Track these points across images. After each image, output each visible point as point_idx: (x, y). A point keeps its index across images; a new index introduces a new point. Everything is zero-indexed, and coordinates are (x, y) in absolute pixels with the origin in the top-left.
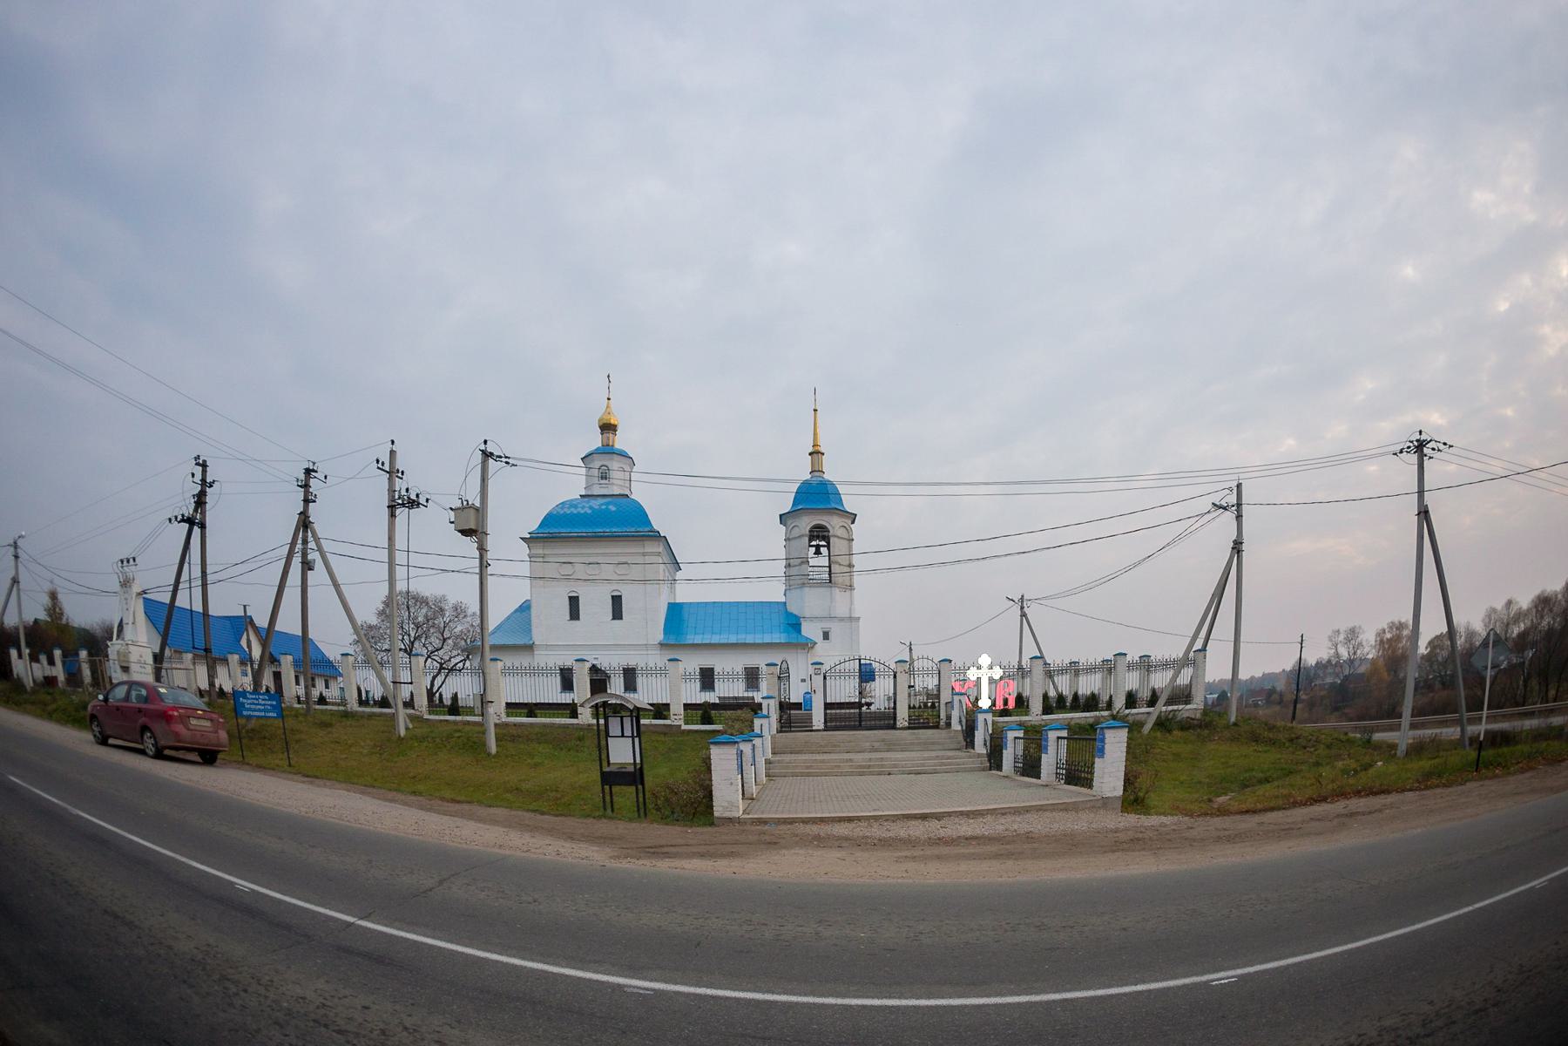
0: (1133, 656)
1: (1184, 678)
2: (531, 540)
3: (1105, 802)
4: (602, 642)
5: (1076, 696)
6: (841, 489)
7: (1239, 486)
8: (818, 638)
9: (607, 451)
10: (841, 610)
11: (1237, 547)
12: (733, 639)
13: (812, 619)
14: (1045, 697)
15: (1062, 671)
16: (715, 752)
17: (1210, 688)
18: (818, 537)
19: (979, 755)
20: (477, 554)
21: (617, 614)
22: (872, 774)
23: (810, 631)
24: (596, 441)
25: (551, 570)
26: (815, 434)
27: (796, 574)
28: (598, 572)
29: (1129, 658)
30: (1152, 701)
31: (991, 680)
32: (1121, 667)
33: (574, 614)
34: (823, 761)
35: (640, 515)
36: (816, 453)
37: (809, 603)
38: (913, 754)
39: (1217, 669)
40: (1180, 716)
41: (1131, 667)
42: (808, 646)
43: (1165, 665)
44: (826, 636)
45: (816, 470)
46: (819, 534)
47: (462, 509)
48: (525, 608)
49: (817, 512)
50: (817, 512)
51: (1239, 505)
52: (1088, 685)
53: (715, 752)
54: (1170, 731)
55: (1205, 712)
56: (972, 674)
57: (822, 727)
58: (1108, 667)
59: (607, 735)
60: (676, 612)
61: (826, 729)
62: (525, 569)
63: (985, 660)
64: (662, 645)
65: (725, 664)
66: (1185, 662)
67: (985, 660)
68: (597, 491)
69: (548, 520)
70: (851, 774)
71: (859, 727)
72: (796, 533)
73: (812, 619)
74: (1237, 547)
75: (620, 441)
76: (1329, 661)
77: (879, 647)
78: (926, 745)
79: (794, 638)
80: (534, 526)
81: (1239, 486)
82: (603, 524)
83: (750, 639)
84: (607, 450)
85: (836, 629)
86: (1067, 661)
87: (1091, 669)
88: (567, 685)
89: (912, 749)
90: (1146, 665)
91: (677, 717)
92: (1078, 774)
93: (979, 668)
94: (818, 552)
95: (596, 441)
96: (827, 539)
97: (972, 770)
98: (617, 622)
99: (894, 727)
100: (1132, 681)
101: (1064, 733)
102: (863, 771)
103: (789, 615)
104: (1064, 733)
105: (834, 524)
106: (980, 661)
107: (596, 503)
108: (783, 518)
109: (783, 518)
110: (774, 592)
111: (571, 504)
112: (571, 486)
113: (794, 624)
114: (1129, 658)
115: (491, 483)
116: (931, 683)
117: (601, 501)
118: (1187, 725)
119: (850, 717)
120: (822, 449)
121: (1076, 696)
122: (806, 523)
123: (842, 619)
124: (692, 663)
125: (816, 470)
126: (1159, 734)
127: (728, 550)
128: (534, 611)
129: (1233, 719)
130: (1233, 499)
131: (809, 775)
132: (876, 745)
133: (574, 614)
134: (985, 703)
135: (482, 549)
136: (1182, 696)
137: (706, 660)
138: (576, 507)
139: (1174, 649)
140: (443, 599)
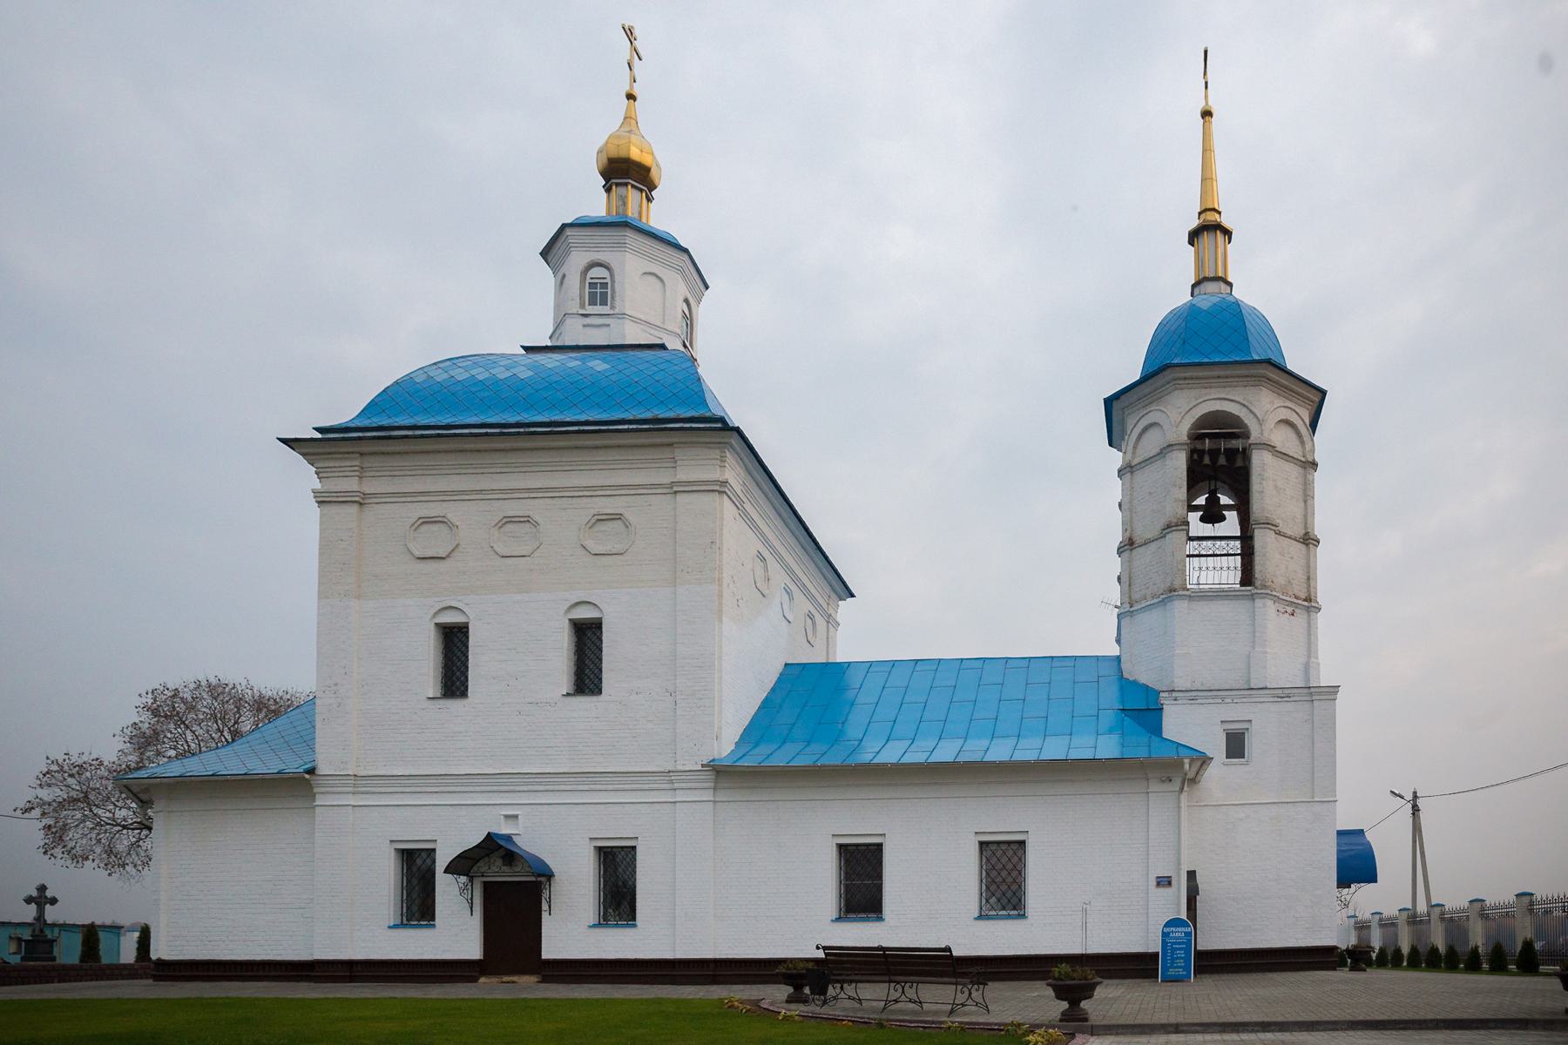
2: (325, 446)
8: (1215, 746)
10: (1281, 669)
13: (1194, 695)
21: (587, 676)
23: (1188, 726)
24: (596, 204)
26: (1207, 179)
27: (1148, 592)
28: (522, 558)
37: (1194, 648)
44: (1236, 745)
49: (1213, 423)
50: (1213, 423)
64: (722, 774)
68: (577, 334)
73: (1194, 695)
75: (659, 216)
79: (1139, 749)
85: (1264, 724)
88: (418, 905)
98: (455, 705)
103: (1127, 686)
105: (1264, 413)
110: (1092, 632)
112: (502, 315)
113: (1143, 710)
120: (1226, 221)
122: (1179, 414)
123: (1283, 695)
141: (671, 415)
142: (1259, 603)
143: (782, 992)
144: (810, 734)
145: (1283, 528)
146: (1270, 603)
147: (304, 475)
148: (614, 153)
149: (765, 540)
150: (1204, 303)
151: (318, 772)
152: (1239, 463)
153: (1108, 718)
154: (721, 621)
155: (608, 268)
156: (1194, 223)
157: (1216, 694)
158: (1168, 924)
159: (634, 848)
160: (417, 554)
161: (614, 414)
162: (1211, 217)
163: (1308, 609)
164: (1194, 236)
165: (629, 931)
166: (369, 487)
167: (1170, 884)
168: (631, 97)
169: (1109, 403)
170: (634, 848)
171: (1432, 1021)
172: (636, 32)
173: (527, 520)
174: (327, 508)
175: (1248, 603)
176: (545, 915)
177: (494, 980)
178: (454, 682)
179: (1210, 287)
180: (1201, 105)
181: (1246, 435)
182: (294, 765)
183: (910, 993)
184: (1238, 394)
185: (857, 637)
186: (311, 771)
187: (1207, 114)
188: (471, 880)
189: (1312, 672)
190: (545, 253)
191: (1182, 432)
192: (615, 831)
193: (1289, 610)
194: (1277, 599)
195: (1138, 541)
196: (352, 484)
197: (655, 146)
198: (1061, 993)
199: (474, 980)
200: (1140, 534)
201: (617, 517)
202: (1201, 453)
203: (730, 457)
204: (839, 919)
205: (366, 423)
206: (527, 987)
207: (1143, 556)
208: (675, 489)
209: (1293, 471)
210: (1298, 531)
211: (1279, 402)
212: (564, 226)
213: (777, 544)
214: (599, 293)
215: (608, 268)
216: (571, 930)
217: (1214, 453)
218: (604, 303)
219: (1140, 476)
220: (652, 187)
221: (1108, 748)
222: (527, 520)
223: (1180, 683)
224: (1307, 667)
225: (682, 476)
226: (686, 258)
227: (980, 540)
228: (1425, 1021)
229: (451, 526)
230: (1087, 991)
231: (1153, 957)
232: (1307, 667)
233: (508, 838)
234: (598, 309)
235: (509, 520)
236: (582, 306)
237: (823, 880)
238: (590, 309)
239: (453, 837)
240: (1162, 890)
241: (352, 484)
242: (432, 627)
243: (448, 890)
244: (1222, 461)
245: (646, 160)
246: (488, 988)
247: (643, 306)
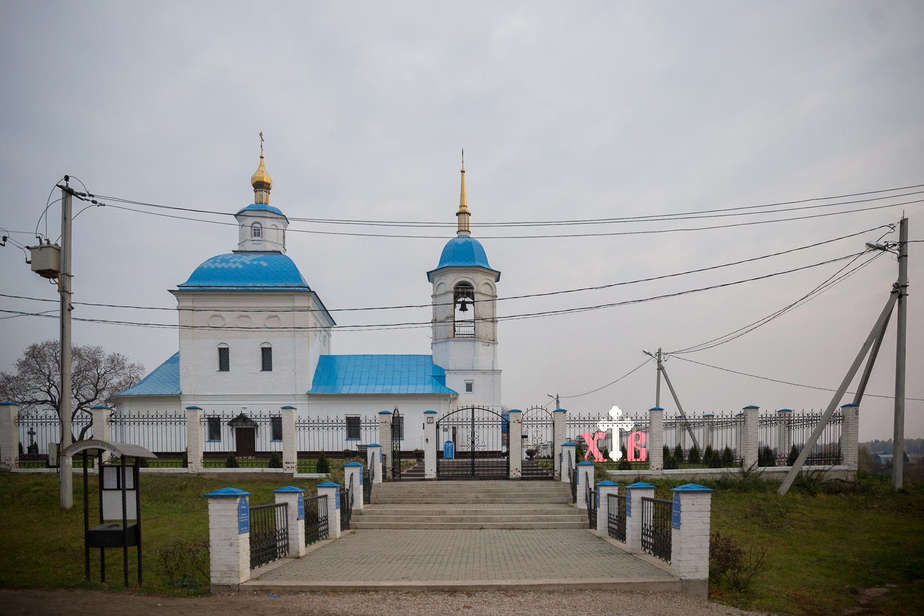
0: (769, 408)
1: (831, 435)
2: (181, 292)
3: (685, 587)
4: (244, 391)
5: (709, 449)
6: (479, 240)
7: (904, 223)
9: (260, 209)
11: (899, 291)
12: (379, 390)
14: (666, 450)
15: (699, 424)
16: (214, 508)
17: (863, 451)
18: (463, 293)
19: (580, 511)
20: (58, 297)
21: (267, 365)
22: (463, 528)
23: (454, 383)
24: (249, 198)
25: (201, 318)
26: (462, 195)
27: (445, 329)
29: (761, 412)
30: (791, 460)
31: (622, 434)
32: (657, 425)
33: (224, 365)
34: (414, 513)
35: (292, 272)
36: (462, 213)
37: (455, 356)
38: (515, 507)
39: (874, 426)
40: (826, 478)
41: (766, 421)
42: (451, 397)
43: (808, 420)
44: (469, 387)
45: (463, 229)
46: (464, 292)
47: (41, 247)
48: (174, 360)
49: (463, 273)
50: (463, 273)
51: (903, 243)
52: (722, 440)
54: (813, 494)
55: (860, 474)
57: (434, 475)
58: (740, 420)
59: (102, 487)
60: (328, 366)
61: (440, 477)
62: (174, 317)
63: (615, 412)
64: (310, 396)
65: (367, 412)
66: (830, 417)
67: (615, 412)
68: (249, 246)
69: (196, 275)
70: (441, 527)
71: (473, 476)
72: (442, 289)
74: (899, 291)
75: (274, 200)
76: (80, 350)
77: (510, 398)
78: (532, 498)
79: (437, 390)
80: (184, 279)
81: (904, 223)
82: (252, 280)
83: (395, 390)
84: (261, 208)
85: (478, 381)
86: (700, 414)
87: (726, 423)
89: (514, 501)
90: (785, 419)
91: (196, 465)
92: (660, 544)
93: (610, 419)
94: (464, 309)
95: (249, 198)
96: (471, 295)
97: (571, 527)
99: (506, 477)
100: (770, 438)
101: (651, 494)
102: (454, 524)
103: (436, 367)
104: (651, 494)
105: (478, 281)
107: (247, 259)
108: (431, 276)
109: (431, 276)
110: (418, 342)
111: (224, 259)
112: (222, 241)
113: (439, 377)
114: (761, 412)
115: (75, 224)
116: (546, 435)
117: (253, 256)
118: (835, 488)
119: (470, 466)
120: (469, 210)
121: (709, 449)
122: (451, 281)
123: (484, 372)
124: (341, 412)
125: (463, 229)
126: (798, 496)
127: (377, 305)
128: (182, 363)
129: (899, 485)
130: (895, 237)
131: (397, 527)
132: (481, 496)
133: (224, 365)
134: (616, 455)
135: (64, 292)
136: (833, 455)
137: (353, 410)
138: (227, 262)
139: (817, 403)
140: (98, 351)
147: (173, 301)
149: (317, 319)
150: (460, 241)
153: (429, 378)
162: (463, 208)
164: (458, 214)
168: (262, 157)
173: (247, 316)
175: (472, 343)
179: (463, 233)
180: (461, 169)
181: (473, 288)
182: (174, 392)
187: (463, 172)
196: (189, 304)
203: (311, 299)
205: (192, 284)
211: (484, 277)
214: (257, 232)
216: (264, 442)
220: (269, 189)
221: (428, 389)
222: (247, 316)
224: (493, 362)
229: (223, 318)
232: (493, 362)
234: (257, 238)
238: (255, 238)
241: (189, 304)
243: (225, 430)
247: (270, 240)
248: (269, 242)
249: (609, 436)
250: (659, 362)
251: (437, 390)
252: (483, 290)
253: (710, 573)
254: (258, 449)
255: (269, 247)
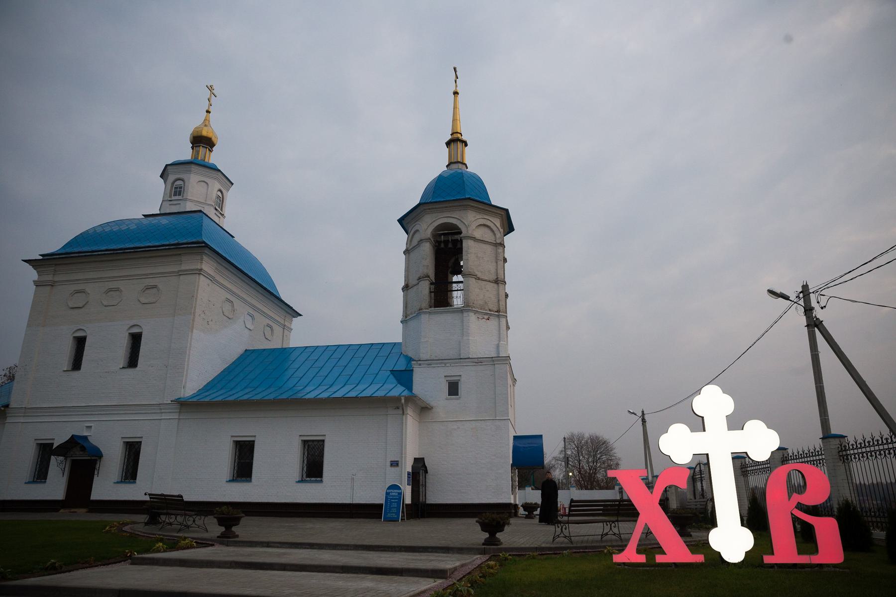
2: (45, 263)
13: (430, 362)
24: (186, 153)
36: (455, 141)
44: (453, 389)
45: (455, 162)
49: (452, 230)
50: (452, 230)
53: (52, 457)
56: (678, 445)
67: (713, 403)
69: (623, 550)
73: (430, 362)
75: (215, 158)
85: (468, 377)
95: (186, 153)
98: (76, 374)
105: (471, 223)
106: (700, 405)
110: (394, 333)
112: (140, 198)
120: (464, 138)
122: (427, 226)
123: (479, 361)
141: (185, 241)
142: (465, 314)
143: (144, 518)
144: (263, 384)
145: (479, 275)
146: (472, 314)
147: (32, 274)
148: (196, 134)
151: (13, 405)
152: (459, 246)
154: (192, 332)
155: (183, 180)
156: (449, 137)
157: (442, 361)
158: (389, 488)
159: (323, 441)
160: (71, 306)
161: (177, 241)
162: (455, 136)
163: (498, 316)
164: (448, 144)
165: (132, 486)
166: (56, 279)
167: (397, 465)
168: (208, 112)
169: (507, 210)
170: (323, 441)
171: (398, 547)
172: (214, 87)
174: (40, 288)
176: (95, 476)
177: (67, 511)
178: (133, 361)
179: (454, 166)
180: (454, 89)
181: (460, 233)
183: (180, 519)
184: (456, 214)
185: (300, 335)
186: (7, 406)
187: (456, 93)
188: (66, 459)
189: (501, 349)
190: (162, 176)
191: (428, 233)
192: (132, 434)
193: (486, 317)
194: (476, 312)
195: (410, 285)
196: (49, 278)
197: (217, 130)
198: (485, 527)
199: (57, 510)
200: (413, 282)
201: (155, 287)
202: (439, 242)
204: (302, 481)
206: (81, 515)
207: (412, 292)
208: (179, 274)
209: (489, 249)
210: (493, 277)
212: (167, 165)
213: (245, 296)
215: (183, 180)
216: (106, 486)
217: (446, 242)
218: (180, 195)
219: (412, 255)
223: (423, 356)
224: (498, 346)
225: (184, 267)
226: (219, 174)
227: (349, 287)
228: (394, 547)
230: (236, 521)
231: (381, 506)
232: (498, 346)
233: (85, 438)
234: (177, 197)
235: (111, 290)
236: (170, 196)
237: (224, 459)
238: (173, 198)
239: (59, 438)
240: (393, 469)
241: (49, 278)
242: (71, 338)
244: (450, 245)
245: (210, 135)
246: (63, 515)
247: (198, 192)
248: (191, 201)
249: (700, 470)
250: (808, 310)
251: (398, 391)
252: (479, 233)
253: (461, 249)
254: (95, 495)
255: (190, 207)
